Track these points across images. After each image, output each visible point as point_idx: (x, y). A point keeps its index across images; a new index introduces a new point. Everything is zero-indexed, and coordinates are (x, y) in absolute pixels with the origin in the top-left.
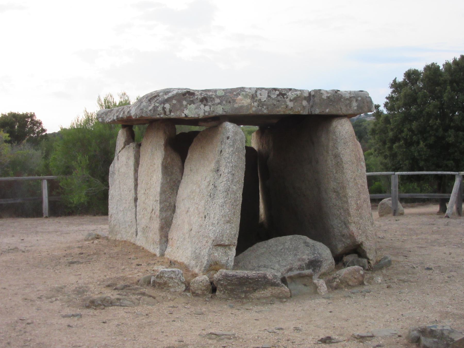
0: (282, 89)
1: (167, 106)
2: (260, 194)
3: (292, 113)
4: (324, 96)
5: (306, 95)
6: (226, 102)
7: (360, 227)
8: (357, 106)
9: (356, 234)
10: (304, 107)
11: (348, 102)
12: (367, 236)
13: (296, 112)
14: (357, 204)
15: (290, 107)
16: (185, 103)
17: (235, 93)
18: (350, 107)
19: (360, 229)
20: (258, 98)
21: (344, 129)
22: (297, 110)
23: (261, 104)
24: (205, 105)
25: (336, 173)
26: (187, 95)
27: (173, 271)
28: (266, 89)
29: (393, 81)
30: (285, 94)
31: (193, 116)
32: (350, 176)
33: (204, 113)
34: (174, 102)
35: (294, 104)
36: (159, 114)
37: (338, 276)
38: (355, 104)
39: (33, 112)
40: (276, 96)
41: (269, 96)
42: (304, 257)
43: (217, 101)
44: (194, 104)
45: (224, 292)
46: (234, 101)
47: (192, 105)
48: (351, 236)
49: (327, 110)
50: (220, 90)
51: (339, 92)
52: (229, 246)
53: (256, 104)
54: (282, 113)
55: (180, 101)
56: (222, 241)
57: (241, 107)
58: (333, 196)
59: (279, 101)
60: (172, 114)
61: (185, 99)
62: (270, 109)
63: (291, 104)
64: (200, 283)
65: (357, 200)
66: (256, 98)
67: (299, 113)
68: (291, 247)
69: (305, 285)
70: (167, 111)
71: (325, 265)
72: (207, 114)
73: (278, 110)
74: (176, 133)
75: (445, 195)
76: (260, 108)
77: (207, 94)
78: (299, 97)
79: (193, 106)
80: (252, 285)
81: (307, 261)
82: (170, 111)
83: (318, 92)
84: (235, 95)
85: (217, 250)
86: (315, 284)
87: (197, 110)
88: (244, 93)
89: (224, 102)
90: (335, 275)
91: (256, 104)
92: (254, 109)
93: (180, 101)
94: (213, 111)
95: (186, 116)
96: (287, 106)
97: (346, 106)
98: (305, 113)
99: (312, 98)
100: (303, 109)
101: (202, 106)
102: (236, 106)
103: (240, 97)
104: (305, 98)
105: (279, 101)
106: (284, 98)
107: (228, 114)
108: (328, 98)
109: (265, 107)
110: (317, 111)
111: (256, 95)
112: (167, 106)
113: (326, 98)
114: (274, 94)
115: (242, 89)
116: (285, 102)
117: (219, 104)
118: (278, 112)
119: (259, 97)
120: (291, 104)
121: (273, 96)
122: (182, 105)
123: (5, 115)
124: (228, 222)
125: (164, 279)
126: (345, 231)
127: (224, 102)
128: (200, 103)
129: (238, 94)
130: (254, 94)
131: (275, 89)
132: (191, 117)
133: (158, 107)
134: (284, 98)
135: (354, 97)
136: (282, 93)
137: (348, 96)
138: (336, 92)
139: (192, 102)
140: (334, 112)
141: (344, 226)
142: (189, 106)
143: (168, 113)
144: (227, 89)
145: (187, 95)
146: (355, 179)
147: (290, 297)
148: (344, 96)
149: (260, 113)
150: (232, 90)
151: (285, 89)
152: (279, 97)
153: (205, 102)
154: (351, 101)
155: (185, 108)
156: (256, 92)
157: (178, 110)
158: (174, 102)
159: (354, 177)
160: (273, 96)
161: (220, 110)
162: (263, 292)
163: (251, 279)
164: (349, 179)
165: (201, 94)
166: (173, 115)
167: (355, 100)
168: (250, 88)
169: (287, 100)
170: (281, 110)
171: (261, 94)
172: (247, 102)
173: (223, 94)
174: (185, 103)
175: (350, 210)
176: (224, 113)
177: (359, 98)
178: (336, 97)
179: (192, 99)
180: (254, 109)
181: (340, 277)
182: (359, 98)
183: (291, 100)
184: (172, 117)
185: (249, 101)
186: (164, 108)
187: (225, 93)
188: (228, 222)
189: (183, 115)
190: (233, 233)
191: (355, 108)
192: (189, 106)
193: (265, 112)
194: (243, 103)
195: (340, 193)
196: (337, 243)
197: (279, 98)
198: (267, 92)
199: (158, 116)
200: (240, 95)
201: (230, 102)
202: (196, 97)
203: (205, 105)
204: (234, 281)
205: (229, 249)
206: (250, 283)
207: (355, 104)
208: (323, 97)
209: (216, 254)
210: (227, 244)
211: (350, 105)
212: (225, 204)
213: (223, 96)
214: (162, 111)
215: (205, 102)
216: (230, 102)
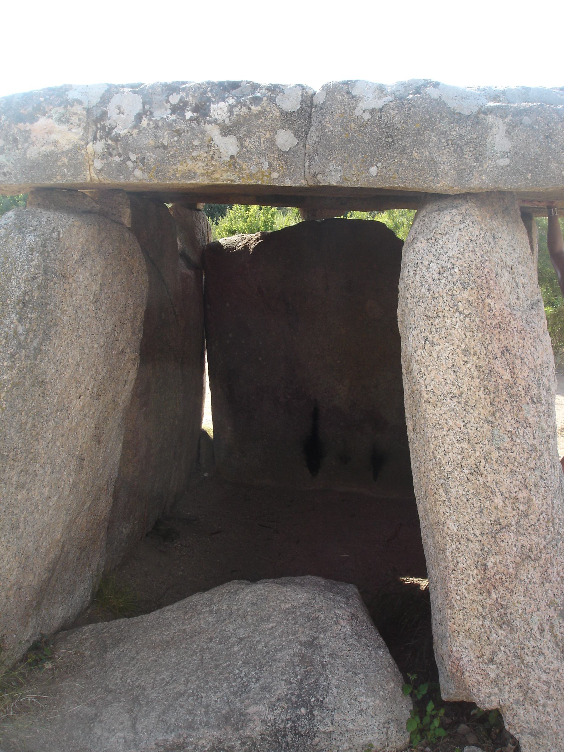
2: (207, 364)
5: (291, 104)
7: (494, 653)
19: (492, 661)
23: (117, 144)
29: (110, 86)
35: (241, 141)
46: (26, 135)
57: (51, 158)
63: (228, 146)
65: (484, 553)
74: (433, 702)
83: (343, 92)
102: (33, 153)
104: (287, 120)
113: (367, 116)
138: (417, 91)
146: (476, 471)
159: (472, 461)
164: (448, 468)
172: (68, 136)
175: (452, 585)
178: (417, 115)
180: (456, 202)
183: (226, 131)
194: (55, 143)
208: (358, 112)
210: (137, 726)
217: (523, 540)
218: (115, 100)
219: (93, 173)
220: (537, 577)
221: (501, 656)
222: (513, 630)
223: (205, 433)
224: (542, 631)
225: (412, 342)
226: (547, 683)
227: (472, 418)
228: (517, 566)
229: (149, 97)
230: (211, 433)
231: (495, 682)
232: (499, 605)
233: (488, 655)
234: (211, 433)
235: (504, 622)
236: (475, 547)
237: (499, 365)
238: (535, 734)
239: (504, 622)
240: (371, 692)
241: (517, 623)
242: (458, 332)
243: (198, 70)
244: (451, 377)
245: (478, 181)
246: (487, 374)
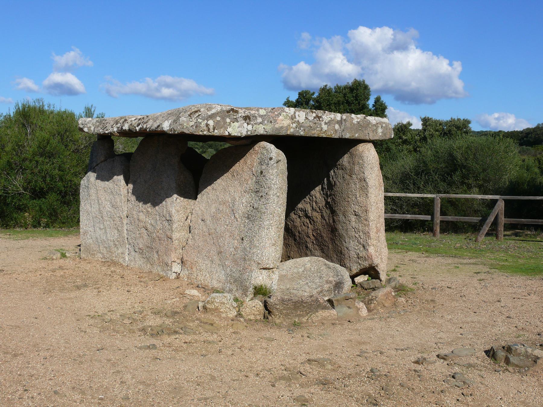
1: (211, 123)
3: (324, 136)
6: (268, 121)
8: (382, 133)
9: (374, 257)
10: (336, 131)
11: (375, 128)
16: (228, 120)
20: (296, 120)
22: (330, 134)
25: (360, 196)
26: (231, 112)
30: (321, 117)
31: (236, 135)
33: (247, 132)
34: (218, 118)
36: (202, 131)
37: (374, 297)
38: (380, 130)
39: (468, 117)
40: (313, 118)
41: (306, 118)
42: (330, 279)
43: (260, 120)
44: (238, 122)
45: (280, 316)
46: (275, 121)
47: (236, 124)
48: (369, 258)
49: (357, 135)
53: (294, 125)
54: (316, 136)
55: (223, 119)
56: (267, 264)
58: (353, 218)
60: (216, 131)
61: (229, 117)
62: (306, 130)
63: (325, 127)
64: (253, 308)
66: (295, 119)
67: (331, 137)
68: (313, 269)
70: (211, 128)
72: (249, 133)
73: (313, 132)
76: (297, 129)
78: (333, 120)
79: (236, 124)
80: (305, 309)
81: (334, 283)
84: (276, 115)
86: (357, 307)
87: (240, 129)
88: (284, 113)
89: (266, 122)
90: (370, 297)
91: (294, 125)
92: (292, 130)
93: (223, 119)
95: (230, 135)
97: (373, 131)
98: (336, 137)
99: (343, 122)
101: (245, 125)
105: (315, 123)
106: (320, 120)
107: (268, 134)
110: (347, 136)
111: (295, 116)
112: (211, 123)
114: (311, 116)
116: (321, 124)
117: (261, 123)
118: (313, 134)
119: (298, 118)
120: (325, 127)
123: (454, 120)
124: (274, 245)
125: (216, 304)
126: (363, 254)
127: (266, 122)
128: (244, 121)
132: (234, 136)
133: (201, 123)
134: (320, 120)
139: (236, 120)
140: (362, 137)
141: (362, 249)
142: (232, 124)
143: (211, 130)
145: (231, 112)
154: (377, 127)
155: (228, 125)
157: (222, 128)
158: (218, 118)
161: (261, 130)
163: (305, 303)
166: (217, 133)
167: (380, 126)
169: (323, 123)
173: (265, 113)
174: (228, 120)
176: (265, 133)
179: (235, 117)
181: (377, 299)
182: (384, 125)
183: (326, 123)
184: (216, 135)
186: (207, 125)
188: (274, 245)
189: (227, 134)
190: (277, 256)
191: (381, 134)
192: (232, 124)
193: (302, 133)
195: (362, 216)
196: (351, 265)
199: (201, 133)
200: (180, 117)
201: (271, 122)
202: (240, 115)
203: (248, 124)
204: (289, 305)
205: (273, 272)
206: (304, 307)
207: (380, 130)
208: (354, 122)
212: (270, 227)
213: (265, 115)
214: (205, 128)
216: (271, 122)
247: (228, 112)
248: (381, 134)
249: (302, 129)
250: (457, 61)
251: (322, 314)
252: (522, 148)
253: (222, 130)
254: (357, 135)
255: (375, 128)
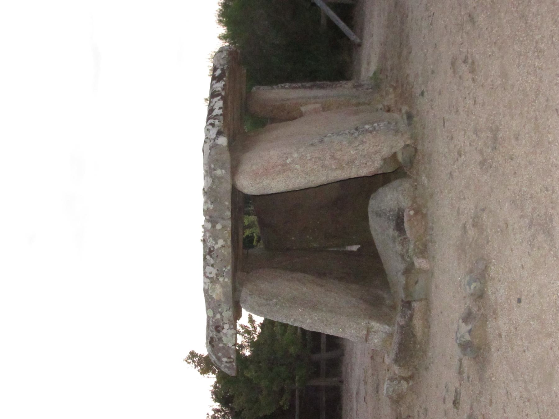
0: (204, 251)
4: (211, 207)
5: (209, 225)
8: (221, 169)
10: (224, 227)
11: (216, 180)
12: (376, 152)
13: (229, 236)
14: (336, 169)
15: (223, 244)
17: (210, 300)
18: (222, 178)
19: (366, 164)
20: (215, 276)
21: (249, 187)
22: (227, 235)
24: (223, 328)
27: (387, 388)
28: (204, 268)
30: (210, 249)
32: (303, 180)
33: (231, 329)
35: (220, 238)
38: (219, 172)
43: (218, 316)
46: (219, 301)
49: (227, 203)
50: (207, 313)
51: (206, 190)
52: (368, 331)
53: (221, 279)
59: (217, 256)
60: (232, 356)
63: (221, 242)
65: (332, 169)
67: (230, 232)
69: (417, 282)
70: (229, 360)
71: (404, 204)
75: (323, 340)
76: (225, 274)
77: (212, 326)
79: (224, 339)
82: (230, 358)
83: (206, 212)
85: (372, 339)
88: (210, 291)
89: (220, 310)
91: (221, 279)
92: (226, 280)
93: (220, 349)
94: (229, 320)
96: (223, 246)
99: (213, 219)
100: (225, 225)
101: (224, 331)
102: (223, 300)
103: (214, 296)
104: (213, 226)
105: (217, 256)
108: (212, 203)
109: (224, 269)
113: (213, 206)
115: (206, 291)
116: (218, 249)
117: (221, 314)
119: (213, 275)
120: (221, 242)
121: (212, 261)
122: (224, 348)
127: (220, 310)
129: (211, 297)
130: (211, 280)
131: (205, 258)
135: (211, 173)
136: (209, 252)
137: (210, 180)
139: (220, 339)
142: (224, 342)
143: (232, 360)
144: (206, 306)
147: (427, 299)
148: (209, 185)
149: (230, 273)
150: (207, 301)
151: (204, 248)
152: (213, 256)
153: (220, 329)
156: (208, 277)
159: (304, 175)
160: (212, 261)
162: (417, 328)
165: (212, 331)
168: (205, 283)
169: (216, 247)
170: (228, 252)
171: (211, 273)
174: (221, 345)
177: (212, 166)
178: (210, 193)
179: (217, 340)
183: (217, 243)
185: (218, 286)
187: (210, 308)
191: (223, 171)
192: (224, 342)
197: (214, 256)
198: (207, 267)
203: (223, 328)
207: (219, 172)
208: (211, 208)
209: (376, 341)
211: (220, 178)
215: (220, 329)
216: (219, 305)
217: (327, 158)
218: (208, 274)
219: (228, 280)
220: (339, 153)
221: (364, 161)
222: (356, 159)
223: (358, 249)
224: (357, 149)
225: (274, 191)
226: (373, 146)
227: (292, 176)
228: (335, 159)
229: (206, 264)
230: (359, 246)
231: (373, 162)
232: (348, 164)
233: (364, 165)
234: (359, 246)
235: (353, 162)
236: (330, 172)
237: (277, 169)
238: (392, 147)
239: (353, 162)
240: (386, 196)
241: (354, 157)
242: (268, 181)
243: (199, 250)
244: (280, 182)
245: (228, 177)
246: (279, 172)
247: (213, 346)
248: (223, 171)
249: (224, 269)
250: (249, 355)
251: (418, 323)
252: (287, 320)
253: (232, 352)
254: (227, 203)
255: (216, 180)
